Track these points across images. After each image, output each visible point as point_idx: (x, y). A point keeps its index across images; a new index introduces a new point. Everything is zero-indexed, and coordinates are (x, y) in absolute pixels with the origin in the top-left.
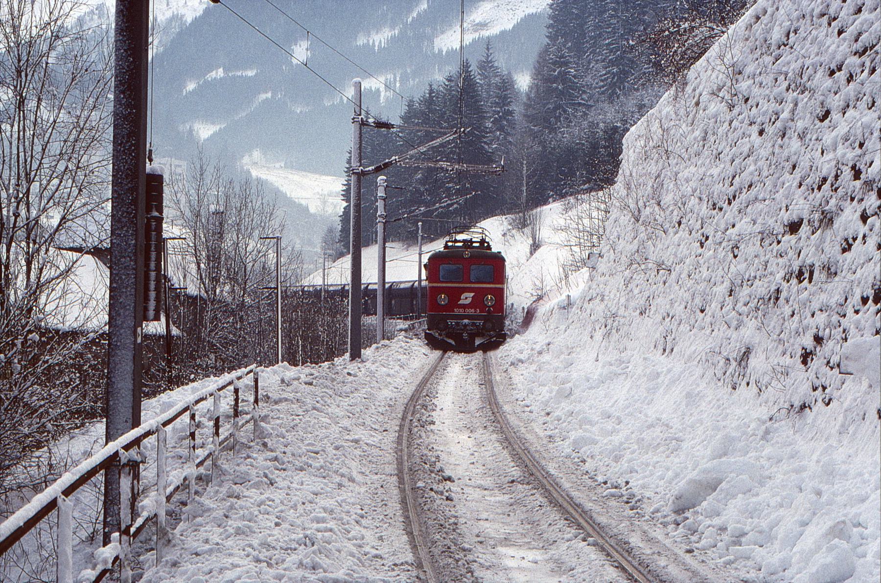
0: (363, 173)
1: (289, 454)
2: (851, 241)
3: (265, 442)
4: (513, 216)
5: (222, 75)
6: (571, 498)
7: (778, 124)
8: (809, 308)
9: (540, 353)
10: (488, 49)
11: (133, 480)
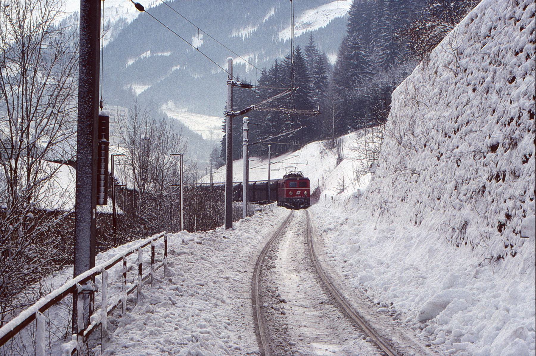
0: (234, 115)
1: (185, 286)
2: (528, 156)
3: (170, 279)
4: (326, 141)
5: (150, 55)
6: (358, 313)
7: (485, 85)
8: (503, 197)
9: (342, 224)
10: (311, 39)
11: (90, 302)
